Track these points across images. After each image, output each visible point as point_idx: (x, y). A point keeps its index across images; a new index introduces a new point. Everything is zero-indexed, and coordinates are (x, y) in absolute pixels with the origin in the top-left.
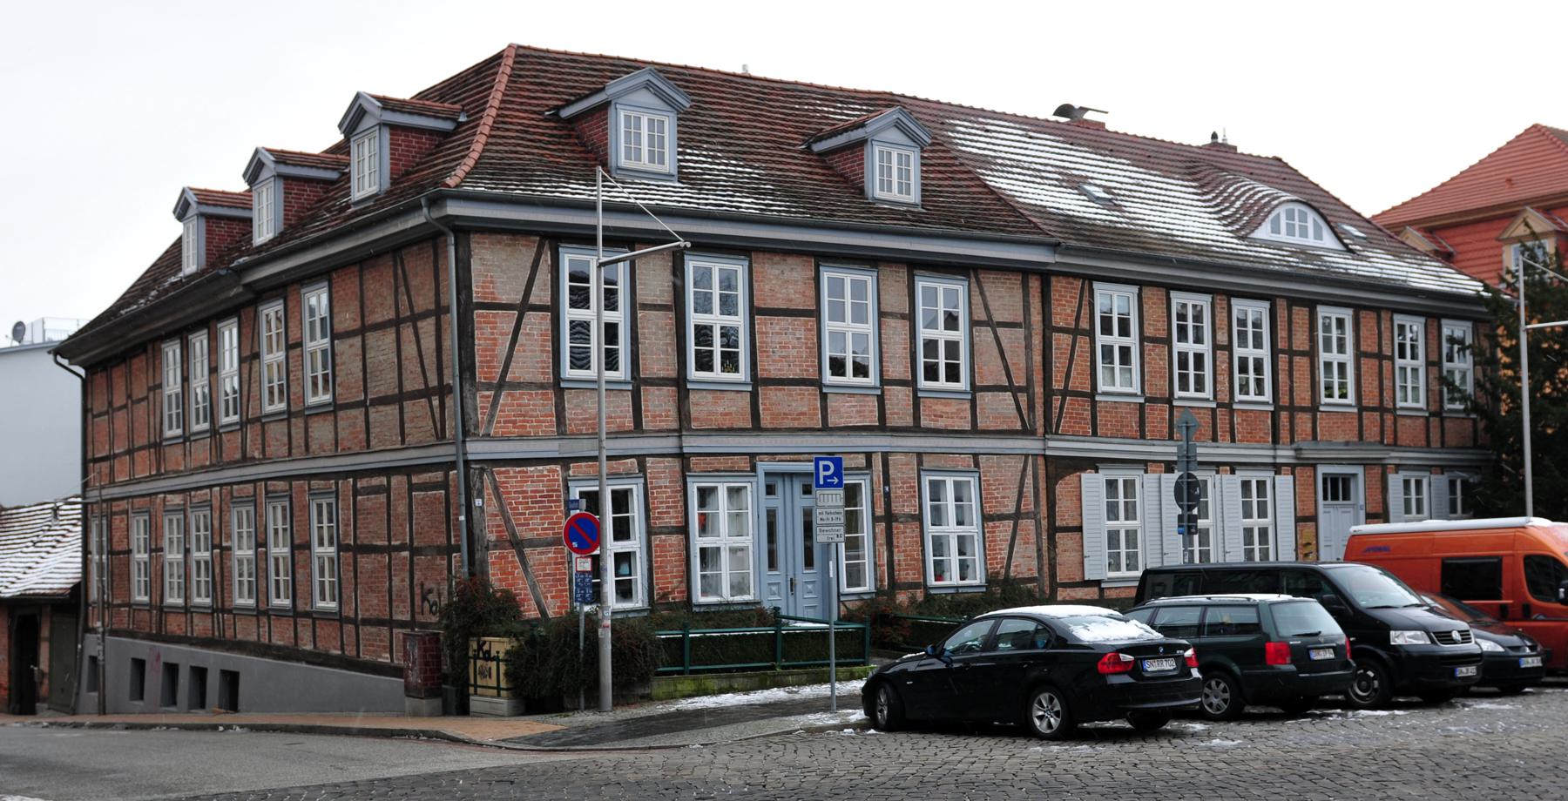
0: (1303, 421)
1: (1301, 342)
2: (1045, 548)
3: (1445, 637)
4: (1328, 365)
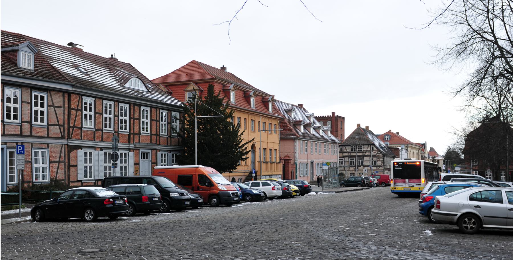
0: (137, 137)
1: (137, 116)
2: (67, 171)
3: (182, 194)
4: (143, 122)
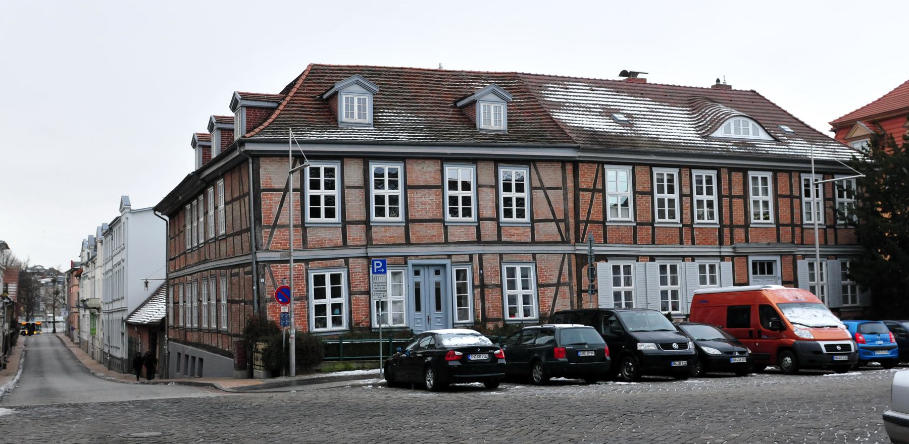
0: (739, 233)
